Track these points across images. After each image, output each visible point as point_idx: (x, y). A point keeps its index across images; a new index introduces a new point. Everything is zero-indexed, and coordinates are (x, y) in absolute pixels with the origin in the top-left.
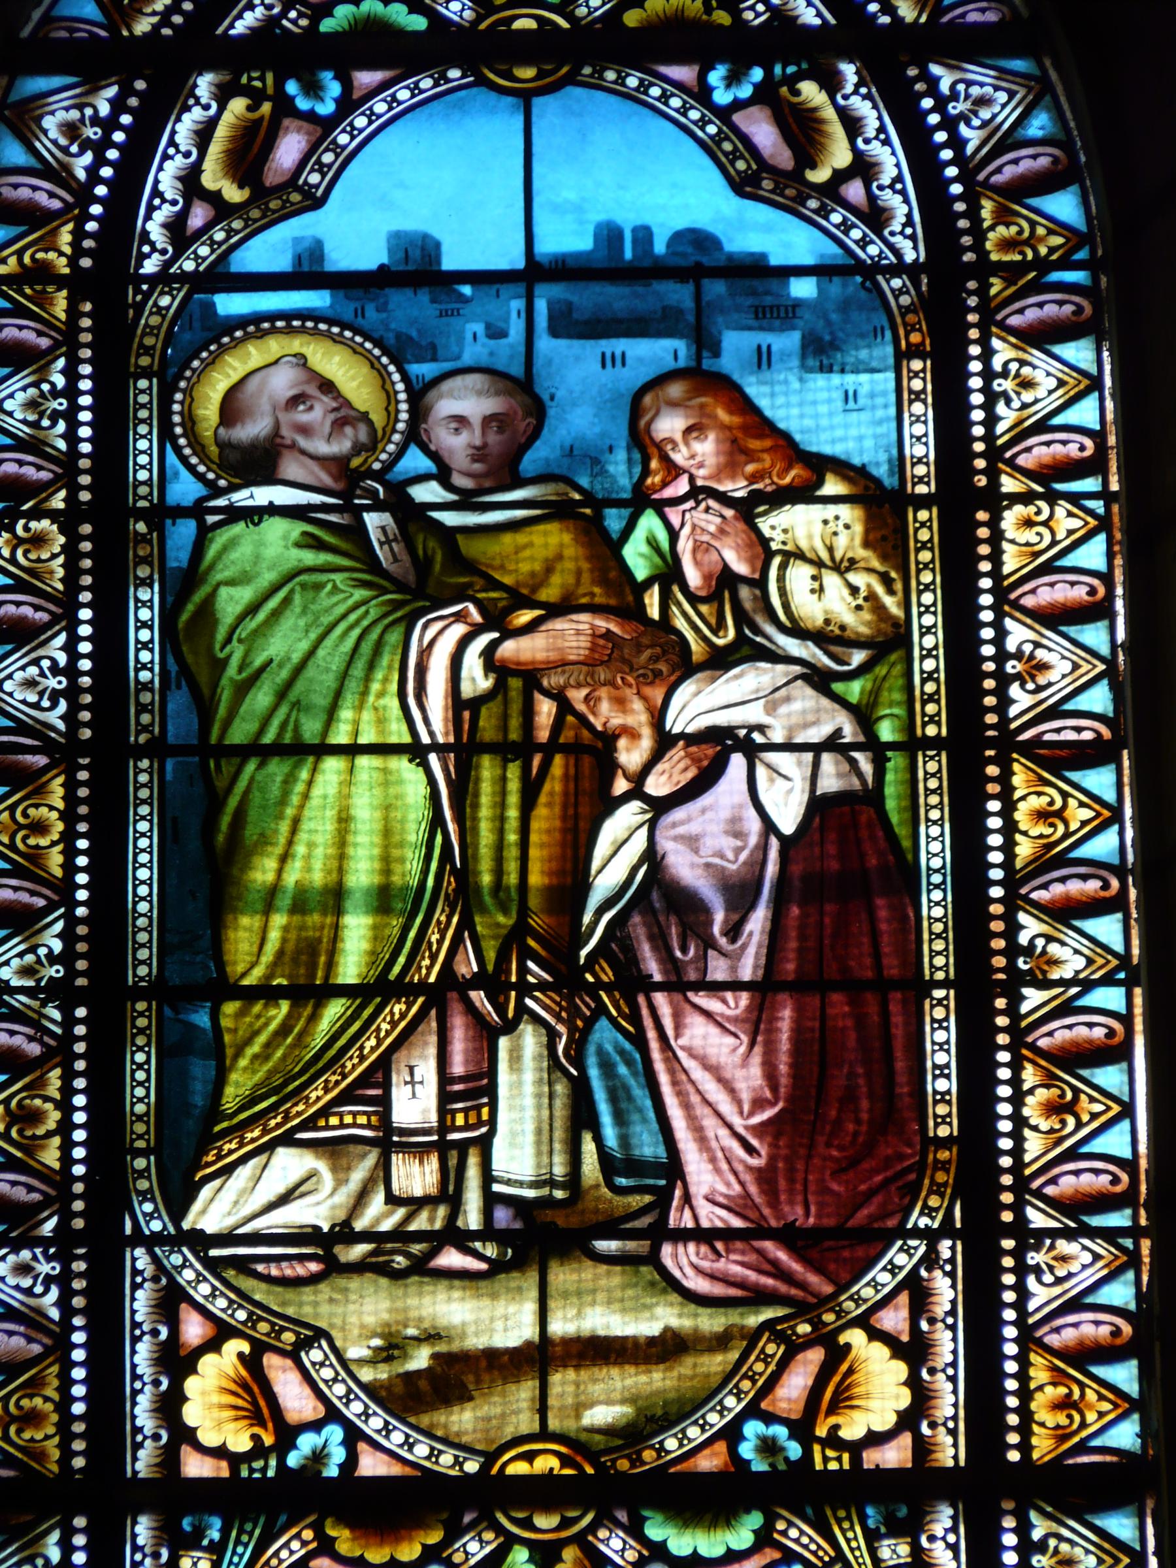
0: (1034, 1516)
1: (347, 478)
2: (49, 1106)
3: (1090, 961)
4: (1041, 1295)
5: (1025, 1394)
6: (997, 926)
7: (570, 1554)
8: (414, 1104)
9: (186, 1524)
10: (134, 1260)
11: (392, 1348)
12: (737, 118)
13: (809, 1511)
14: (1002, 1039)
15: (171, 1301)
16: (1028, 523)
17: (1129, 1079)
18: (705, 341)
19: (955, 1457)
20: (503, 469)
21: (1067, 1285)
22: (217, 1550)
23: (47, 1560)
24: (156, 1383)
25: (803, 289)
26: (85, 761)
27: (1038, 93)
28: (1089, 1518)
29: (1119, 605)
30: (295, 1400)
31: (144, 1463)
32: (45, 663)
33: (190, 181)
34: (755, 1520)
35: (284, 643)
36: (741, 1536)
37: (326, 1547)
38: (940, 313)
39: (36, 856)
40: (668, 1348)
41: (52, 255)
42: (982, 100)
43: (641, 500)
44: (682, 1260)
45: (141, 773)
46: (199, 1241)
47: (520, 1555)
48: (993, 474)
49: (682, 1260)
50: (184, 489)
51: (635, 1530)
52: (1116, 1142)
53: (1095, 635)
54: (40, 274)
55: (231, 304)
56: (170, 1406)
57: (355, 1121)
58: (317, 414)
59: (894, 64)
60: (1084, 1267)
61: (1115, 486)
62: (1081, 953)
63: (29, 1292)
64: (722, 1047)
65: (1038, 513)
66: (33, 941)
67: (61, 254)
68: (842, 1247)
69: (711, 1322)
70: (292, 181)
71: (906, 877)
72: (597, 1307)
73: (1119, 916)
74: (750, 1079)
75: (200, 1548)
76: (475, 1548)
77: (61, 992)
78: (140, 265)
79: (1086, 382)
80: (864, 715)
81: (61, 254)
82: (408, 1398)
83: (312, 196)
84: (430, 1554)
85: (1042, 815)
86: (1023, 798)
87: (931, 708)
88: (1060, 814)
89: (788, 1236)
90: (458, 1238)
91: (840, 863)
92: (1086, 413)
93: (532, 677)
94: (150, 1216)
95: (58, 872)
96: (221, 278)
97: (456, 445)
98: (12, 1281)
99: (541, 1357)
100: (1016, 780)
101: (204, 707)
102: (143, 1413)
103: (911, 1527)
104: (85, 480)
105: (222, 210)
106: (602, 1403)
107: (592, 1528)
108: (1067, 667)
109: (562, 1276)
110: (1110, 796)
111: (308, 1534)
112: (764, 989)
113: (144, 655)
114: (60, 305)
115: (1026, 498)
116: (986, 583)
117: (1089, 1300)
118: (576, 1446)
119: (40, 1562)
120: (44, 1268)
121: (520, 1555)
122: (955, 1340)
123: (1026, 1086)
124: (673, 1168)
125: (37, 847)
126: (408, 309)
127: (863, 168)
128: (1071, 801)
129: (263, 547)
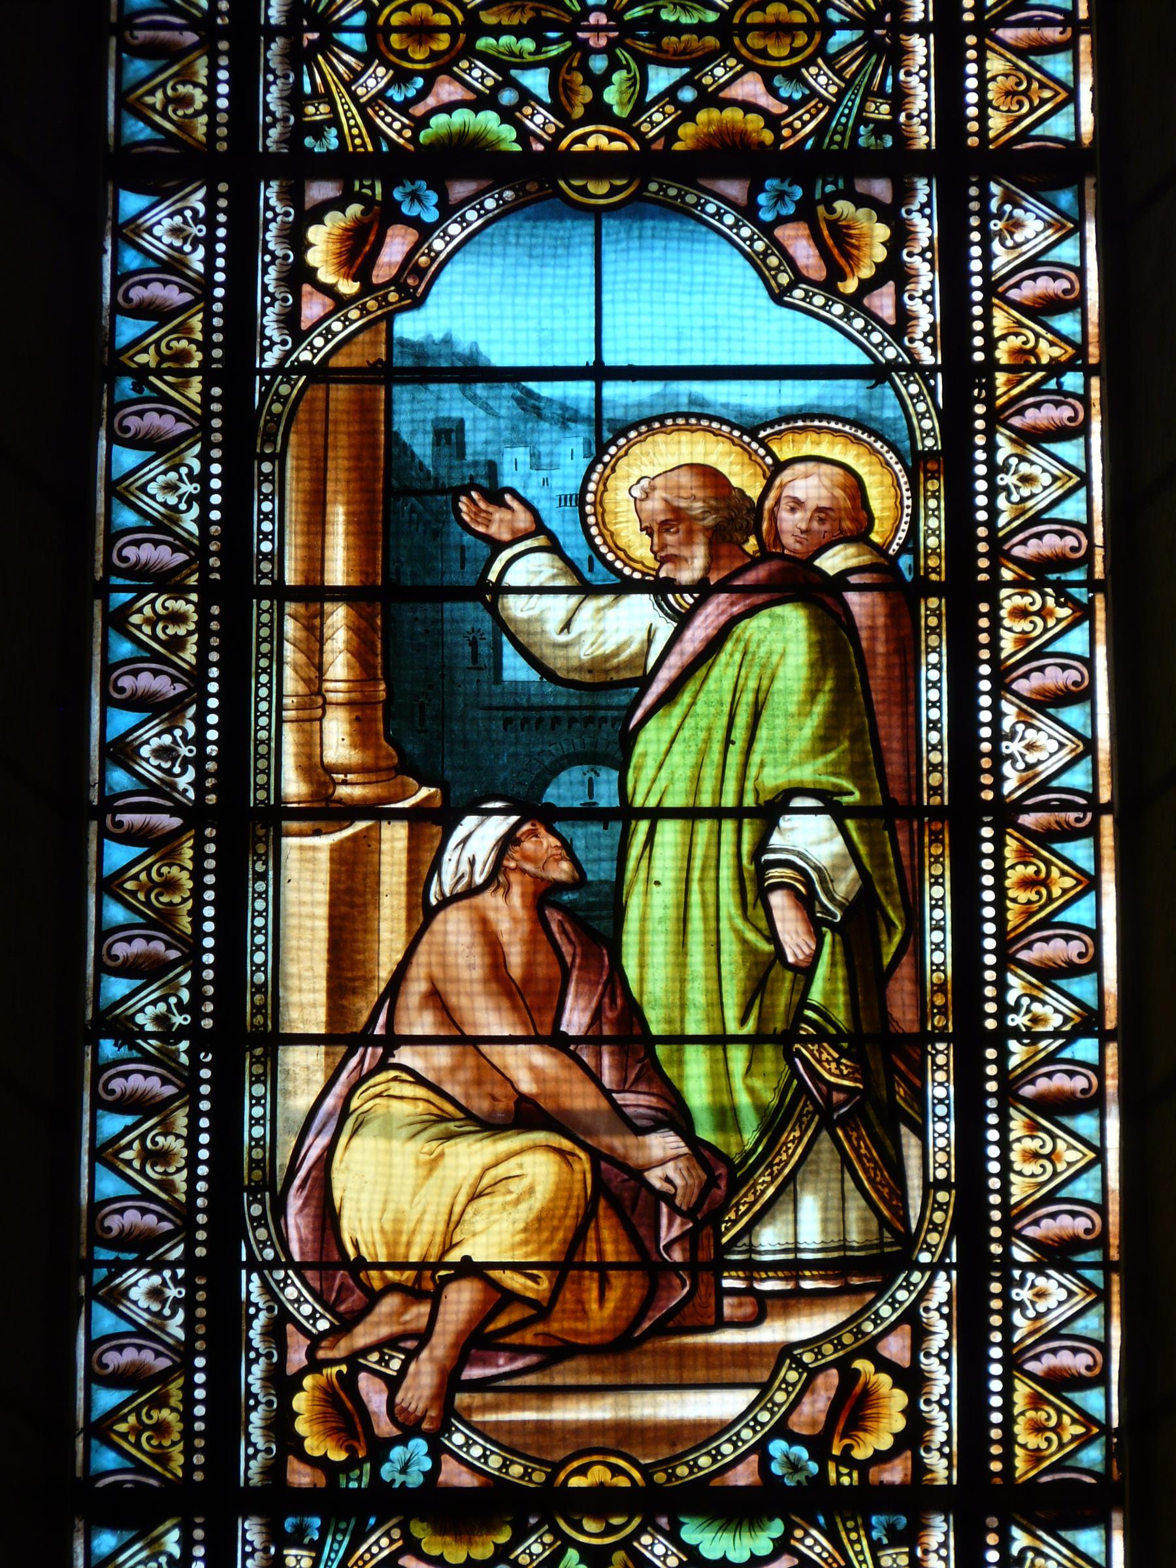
0: (1016, 1532)
2: (181, 1142)
3: (1067, 1019)
4: (1002, 259)
5: (999, 873)
6: (989, 912)
7: (619, 1556)
9: (889, 141)
10: (245, 1531)
12: (778, 232)
13: (822, 1520)
14: (982, 547)
16: (1035, 1156)
19: (949, 1478)
21: (1024, 248)
22: (316, 1547)
23: (170, 1556)
24: (286, 77)
26: (199, 1520)
28: (1063, 1534)
29: (1096, 426)
31: (252, 1471)
32: (184, 471)
34: (777, 1528)
36: (762, 1543)
37: (412, 1547)
41: (175, 870)
47: (572, 1554)
48: (993, 570)
51: (673, 1536)
60: (1060, 1303)
61: (1114, 1254)
63: (168, 772)
65: (1019, 84)
66: (177, 460)
67: (178, 1136)
70: (396, 281)
73: (1081, 440)
75: (300, 1546)
76: (536, 1547)
78: (262, 360)
79: (1064, 94)
81: (183, 868)
83: (412, 296)
84: (502, 1552)
85: (1026, 884)
86: (1019, 1140)
87: (938, 914)
88: (1046, 883)
94: (263, 1244)
95: (189, 930)
98: (154, 762)
100: (1008, 852)
102: (924, 230)
103: (909, 1537)
104: (201, 1235)
105: (869, 1349)
107: (559, 135)
108: (1053, 746)
110: (1088, 866)
111: (396, 1533)
114: (195, 388)
115: (1019, 584)
116: (985, 670)
117: (1064, 1331)
119: (163, 1560)
120: (172, 1292)
121: (572, 1554)
122: (949, 1420)
123: (997, 333)
125: (170, 904)
128: (1060, 1143)
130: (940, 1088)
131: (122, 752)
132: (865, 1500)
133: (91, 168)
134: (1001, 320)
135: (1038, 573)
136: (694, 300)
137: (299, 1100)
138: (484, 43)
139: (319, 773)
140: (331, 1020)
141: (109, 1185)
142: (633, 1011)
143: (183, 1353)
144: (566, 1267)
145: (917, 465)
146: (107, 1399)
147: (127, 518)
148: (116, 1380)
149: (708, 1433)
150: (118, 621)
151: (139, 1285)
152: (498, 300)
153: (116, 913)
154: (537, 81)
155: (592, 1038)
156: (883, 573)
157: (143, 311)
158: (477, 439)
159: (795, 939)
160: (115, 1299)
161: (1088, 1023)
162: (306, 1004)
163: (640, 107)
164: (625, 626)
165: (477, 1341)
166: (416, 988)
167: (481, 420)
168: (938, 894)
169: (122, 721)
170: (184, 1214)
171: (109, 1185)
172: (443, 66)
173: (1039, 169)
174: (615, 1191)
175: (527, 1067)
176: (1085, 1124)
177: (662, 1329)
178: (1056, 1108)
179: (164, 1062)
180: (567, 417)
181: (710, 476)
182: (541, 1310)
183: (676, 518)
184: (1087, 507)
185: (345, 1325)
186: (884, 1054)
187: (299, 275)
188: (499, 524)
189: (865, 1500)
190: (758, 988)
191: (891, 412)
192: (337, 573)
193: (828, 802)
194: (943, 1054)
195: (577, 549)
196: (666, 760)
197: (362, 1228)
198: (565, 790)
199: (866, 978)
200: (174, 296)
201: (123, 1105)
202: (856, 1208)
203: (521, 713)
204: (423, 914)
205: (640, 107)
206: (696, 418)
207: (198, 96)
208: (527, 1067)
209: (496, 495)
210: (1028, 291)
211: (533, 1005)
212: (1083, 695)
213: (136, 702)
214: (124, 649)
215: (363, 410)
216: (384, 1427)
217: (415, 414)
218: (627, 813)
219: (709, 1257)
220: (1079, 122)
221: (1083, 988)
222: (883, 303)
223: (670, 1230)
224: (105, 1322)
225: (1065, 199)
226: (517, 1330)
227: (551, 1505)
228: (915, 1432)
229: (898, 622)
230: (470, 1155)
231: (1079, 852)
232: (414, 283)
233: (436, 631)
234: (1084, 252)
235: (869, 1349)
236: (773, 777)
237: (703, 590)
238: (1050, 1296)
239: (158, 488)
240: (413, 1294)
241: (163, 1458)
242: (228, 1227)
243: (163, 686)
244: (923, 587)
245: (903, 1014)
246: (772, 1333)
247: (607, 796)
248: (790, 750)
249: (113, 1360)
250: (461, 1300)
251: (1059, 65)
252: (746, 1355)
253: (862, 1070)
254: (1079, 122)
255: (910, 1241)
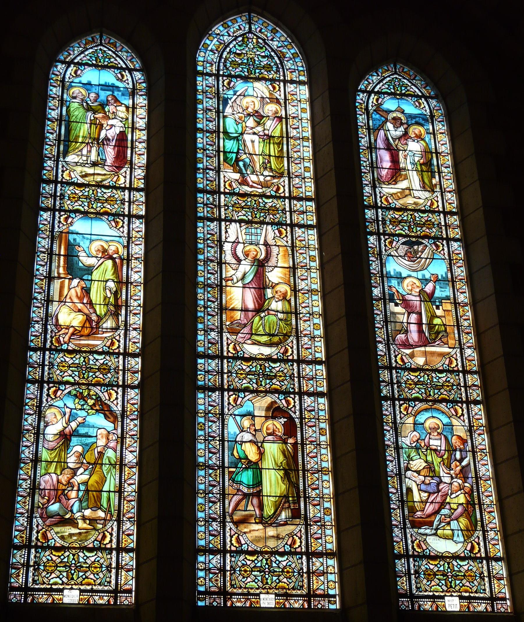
1: (82, 100)
4: (474, 413)
8: (85, 152)
11: (81, 172)
15: (63, 166)
17: (145, 157)
18: (113, 92)
20: (96, 101)
25: (122, 89)
27: (143, 75)
30: (73, 176)
33: (373, 102)
35: (76, 113)
38: (133, 93)
39: (28, 472)
40: (105, 175)
42: (138, 75)
43: (107, 105)
44: (106, 167)
45: (63, 122)
46: (65, 162)
49: (106, 167)
50: (68, 99)
52: (143, 162)
53: (144, 120)
54: (57, 80)
55: (73, 84)
56: (231, 541)
57: (79, 153)
58: (80, 94)
59: (131, 71)
62: (141, 147)
64: (111, 151)
68: (120, 168)
69: (108, 173)
71: (127, 140)
72: (98, 170)
74: (113, 153)
77: (55, 140)
80: (124, 125)
82: (82, 177)
89: (115, 167)
90: (87, 164)
91: (122, 138)
92: (136, 429)
93: (97, 118)
96: (72, 82)
97: (92, 98)
99: (94, 174)
101: (69, 118)
102: (34, 538)
106: (99, 178)
109: (96, 168)
112: (115, 146)
113: (64, 113)
118: (96, 182)
124: (106, 160)
126: (88, 87)
127: (127, 80)
129: (76, 105)
130: (123, 312)
131: (38, 270)
132: (113, 354)
133: (37, 209)
134: (129, 405)
135: (136, 259)
136: (101, 227)
137: (54, 309)
138: (58, 569)
139: (59, 273)
140: (59, 299)
141: (34, 315)
142: (91, 301)
143: (41, 333)
144: (83, 327)
145: (124, 247)
146: (33, 338)
147: (28, 392)
148: (34, 336)
149: (97, 345)
150: (38, 256)
151: (37, 326)
152: (80, 225)
153: (36, 287)
154: (86, 204)
155: (87, 303)
156: (120, 257)
157: (43, 224)
158: (78, 241)
159: (109, 295)
160: (34, 327)
161: (139, 305)
162: (56, 298)
163: (261, 561)
164: (91, 261)
165: (73, 334)
166: (68, 297)
167: (79, 238)
168: (124, 291)
169: (38, 267)
170: (42, 319)
171: (34, 315)
172: (76, 201)
173: (138, 217)
174: (89, 319)
175: (80, 306)
176: (138, 316)
177: (93, 334)
178: (135, 314)
179: (41, 302)
180: (87, 239)
181: (102, 246)
182: (80, 332)
183: (98, 250)
184: (142, 252)
185: (59, 331)
186: (117, 307)
187: (400, 412)
188: (80, 249)
189: (113, 354)
190: (105, 299)
191: (121, 241)
192: (62, 253)
193: (113, 281)
194: (124, 308)
195: (88, 253)
196: (96, 275)
197: (61, 322)
198: (85, 277)
199: (116, 299)
200: (46, 223)
201: (36, 307)
202: (114, 323)
203: (81, 269)
204: (69, 289)
205: (88, 377)
206: (101, 240)
207: (49, 202)
208: (80, 306)
209: (79, 246)
210: (137, 230)
211: (81, 299)
212: (446, 144)
213: (40, 265)
214: (39, 259)
215: (66, 236)
216: (62, 343)
217: (71, 237)
218: (91, 280)
219: (98, 327)
220: (143, 213)
221: (139, 302)
222: (278, 93)
223: (94, 324)
224: (33, 329)
225: (141, 220)
226: (77, 333)
227: (80, 352)
228: (119, 347)
229: (121, 263)
230: (73, 314)
231: (139, 288)
232: (71, 224)
233: (72, 260)
234: (143, 226)
235: (114, 338)
236: (107, 278)
237: (101, 258)
238: (133, 334)
239: (43, 243)
240: (66, 329)
241: (23, 541)
242: (47, 320)
243: (43, 263)
244: (124, 259)
245: (120, 303)
246: (105, 335)
247: (90, 278)
248: (110, 275)
249: (33, 334)
250: (71, 330)
251: (141, 207)
252: (101, 338)
253: (115, 308)
254: (143, 213)
255: (119, 327)
